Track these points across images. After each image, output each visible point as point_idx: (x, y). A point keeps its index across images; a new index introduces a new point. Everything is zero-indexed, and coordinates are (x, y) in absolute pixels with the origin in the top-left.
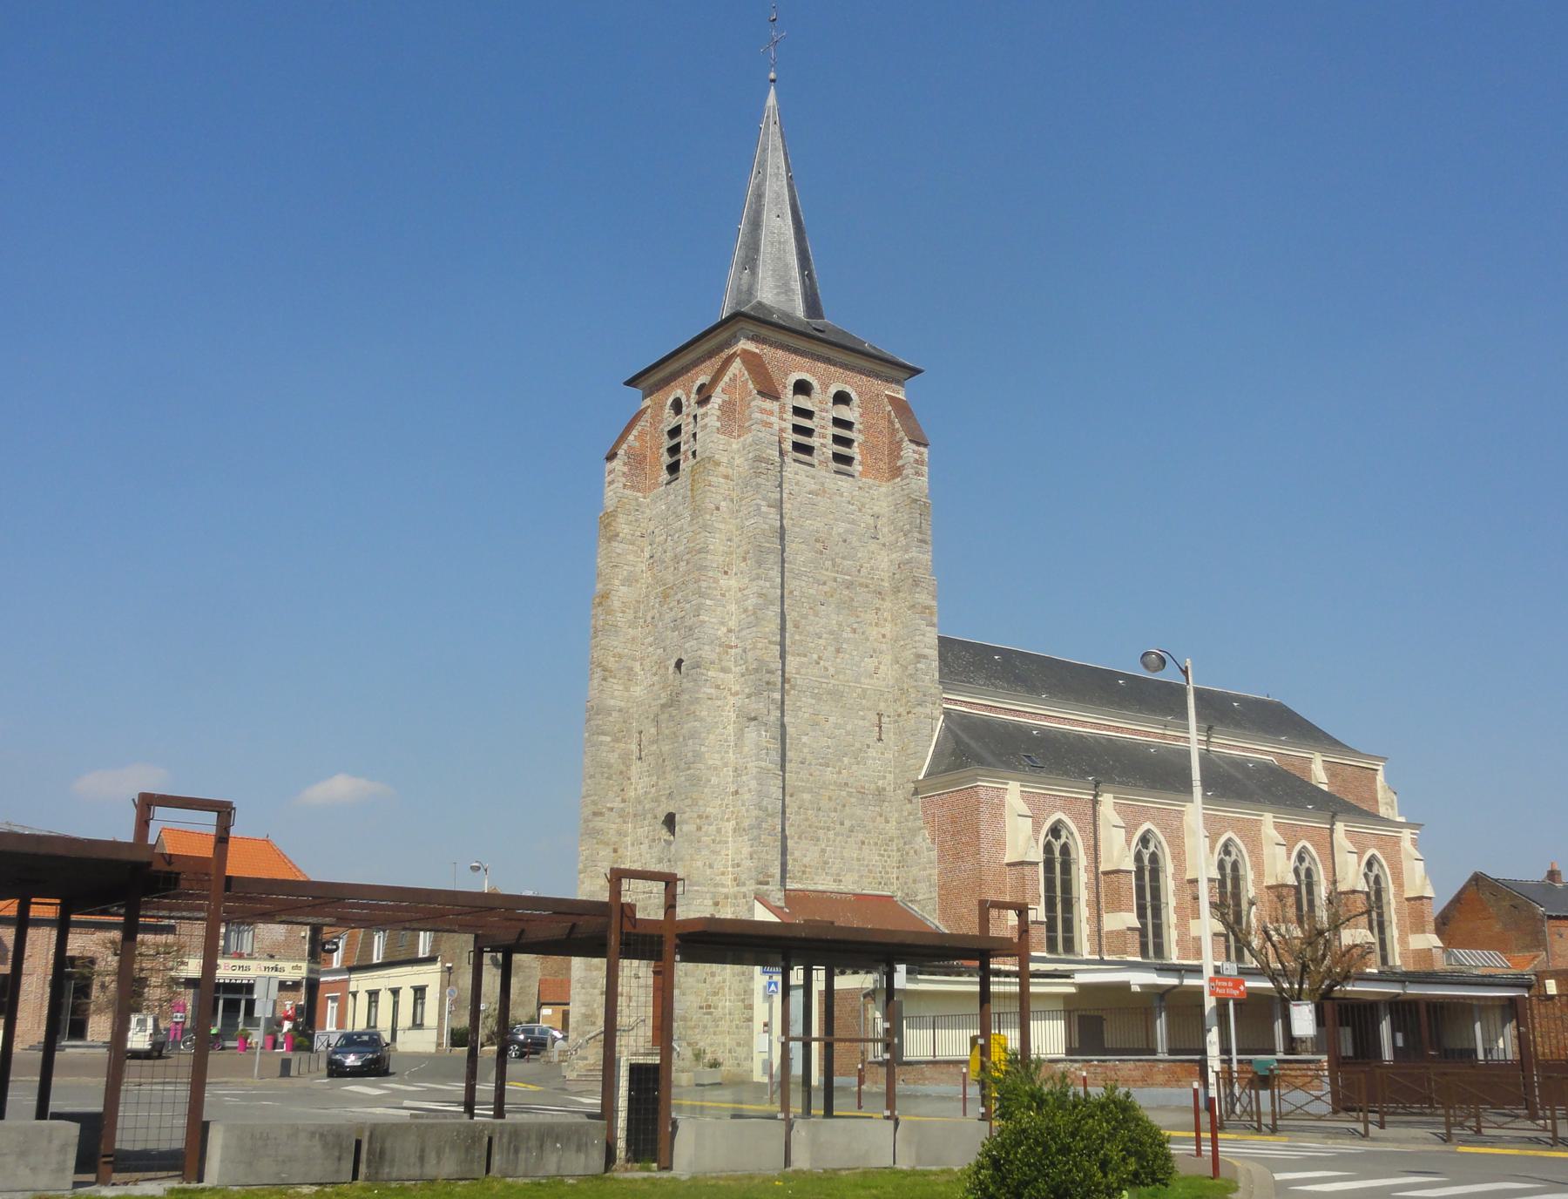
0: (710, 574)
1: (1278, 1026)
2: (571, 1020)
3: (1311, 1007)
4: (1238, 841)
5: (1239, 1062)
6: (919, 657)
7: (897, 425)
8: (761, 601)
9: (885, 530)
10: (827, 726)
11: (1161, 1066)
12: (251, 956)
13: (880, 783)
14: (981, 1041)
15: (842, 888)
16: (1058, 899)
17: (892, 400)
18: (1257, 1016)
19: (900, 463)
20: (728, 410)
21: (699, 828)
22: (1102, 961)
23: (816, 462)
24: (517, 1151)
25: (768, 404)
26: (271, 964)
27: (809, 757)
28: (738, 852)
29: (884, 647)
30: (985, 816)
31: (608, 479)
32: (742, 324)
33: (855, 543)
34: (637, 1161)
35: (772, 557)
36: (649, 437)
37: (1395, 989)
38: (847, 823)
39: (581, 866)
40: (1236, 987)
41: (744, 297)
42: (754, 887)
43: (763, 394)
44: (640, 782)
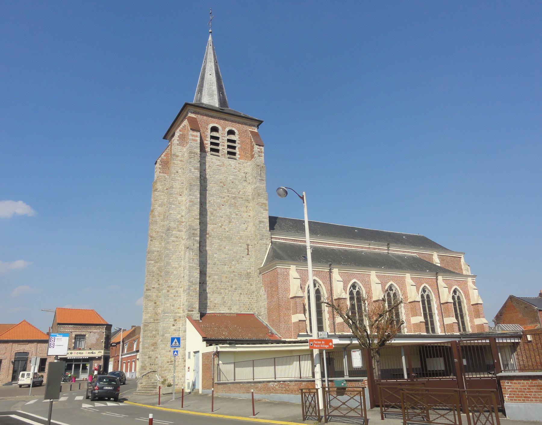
0: (174, 196)
1: (345, 361)
4: (395, 285)
8: (191, 204)
12: (84, 349)
13: (248, 271)
15: (232, 312)
17: (251, 132)
21: (168, 291)
26: (91, 351)
27: (217, 262)
29: (250, 220)
30: (280, 280)
33: (237, 183)
35: (196, 187)
38: (234, 287)
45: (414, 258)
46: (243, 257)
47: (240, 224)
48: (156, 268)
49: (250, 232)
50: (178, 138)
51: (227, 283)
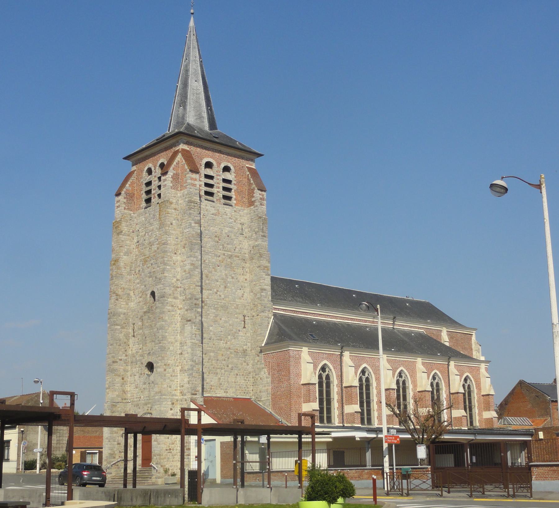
0: (169, 254)
2: (104, 456)
3: (425, 447)
4: (405, 371)
5: (396, 469)
6: (263, 290)
7: (252, 182)
8: (192, 267)
9: (246, 230)
10: (221, 322)
11: (366, 471)
13: (245, 347)
14: (299, 462)
16: (325, 399)
17: (250, 169)
18: (405, 450)
19: (253, 199)
20: (176, 178)
21: (165, 370)
22: (343, 427)
23: (215, 200)
24: (158, 497)
25: (194, 176)
27: (213, 336)
28: (182, 380)
29: (246, 285)
30: (292, 363)
31: (117, 205)
32: (181, 137)
33: (233, 237)
34: (191, 501)
36: (136, 186)
37: (471, 437)
38: (230, 366)
39: (107, 386)
40: (396, 439)
41: (180, 120)
42: (190, 396)
43: (191, 171)
44: (134, 347)
45: (421, 335)
46: (239, 331)
47: (236, 290)
48: (123, 335)
49: (246, 300)
50: (171, 179)
51: (224, 362)
